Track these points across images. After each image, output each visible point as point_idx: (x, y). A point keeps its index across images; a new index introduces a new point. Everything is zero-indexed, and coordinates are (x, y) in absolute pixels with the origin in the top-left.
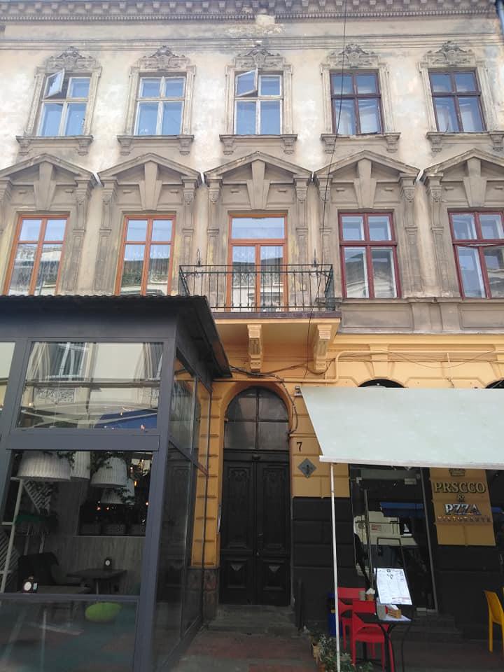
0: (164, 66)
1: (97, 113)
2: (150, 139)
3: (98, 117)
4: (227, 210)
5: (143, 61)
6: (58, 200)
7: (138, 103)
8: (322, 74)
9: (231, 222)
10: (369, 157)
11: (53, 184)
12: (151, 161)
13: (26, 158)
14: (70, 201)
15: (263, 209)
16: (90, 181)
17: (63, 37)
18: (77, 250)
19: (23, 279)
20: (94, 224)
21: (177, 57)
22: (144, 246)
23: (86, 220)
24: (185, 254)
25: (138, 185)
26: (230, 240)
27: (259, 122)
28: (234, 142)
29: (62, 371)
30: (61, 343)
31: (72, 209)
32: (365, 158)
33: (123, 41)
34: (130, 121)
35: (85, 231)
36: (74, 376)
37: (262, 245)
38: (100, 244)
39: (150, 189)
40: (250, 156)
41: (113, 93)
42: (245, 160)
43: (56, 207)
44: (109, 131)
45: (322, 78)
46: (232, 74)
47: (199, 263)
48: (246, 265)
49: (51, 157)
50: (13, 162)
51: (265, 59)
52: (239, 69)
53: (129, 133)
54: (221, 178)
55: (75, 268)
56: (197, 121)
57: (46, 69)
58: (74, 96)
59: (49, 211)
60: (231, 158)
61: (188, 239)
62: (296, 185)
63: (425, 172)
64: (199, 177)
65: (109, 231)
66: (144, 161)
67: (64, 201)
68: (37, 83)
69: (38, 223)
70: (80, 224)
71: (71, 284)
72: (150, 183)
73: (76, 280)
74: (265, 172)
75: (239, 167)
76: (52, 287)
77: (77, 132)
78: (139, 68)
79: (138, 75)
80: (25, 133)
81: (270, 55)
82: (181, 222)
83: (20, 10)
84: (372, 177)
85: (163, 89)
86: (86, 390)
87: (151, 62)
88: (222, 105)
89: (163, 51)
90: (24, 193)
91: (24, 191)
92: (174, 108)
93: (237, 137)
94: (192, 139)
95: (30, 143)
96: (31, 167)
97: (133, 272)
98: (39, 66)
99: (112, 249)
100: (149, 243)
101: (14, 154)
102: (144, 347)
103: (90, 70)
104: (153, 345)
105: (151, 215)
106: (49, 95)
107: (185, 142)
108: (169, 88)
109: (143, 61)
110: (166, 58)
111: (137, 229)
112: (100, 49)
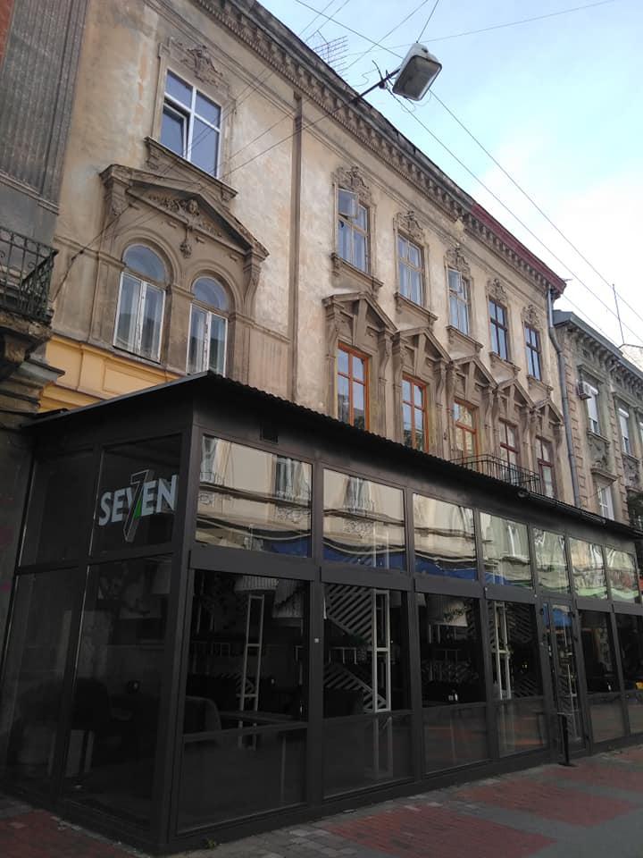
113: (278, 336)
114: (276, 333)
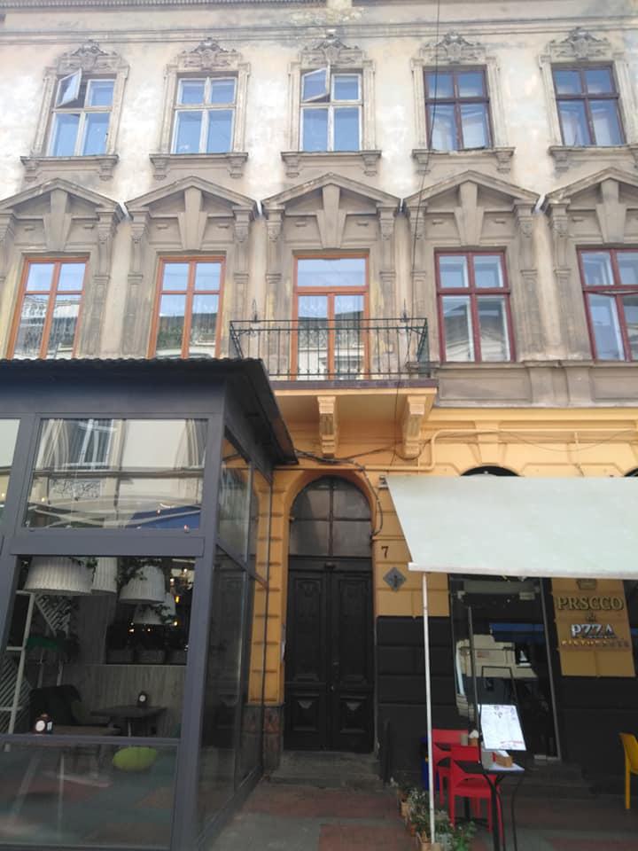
0: (210, 63)
2: (192, 159)
3: (125, 131)
5: (182, 57)
8: (413, 72)
11: (68, 218)
12: (193, 187)
13: (33, 185)
14: (91, 240)
15: (338, 247)
16: (115, 213)
17: (79, 28)
18: (100, 302)
20: (121, 267)
23: (111, 263)
26: (295, 288)
28: (299, 161)
29: (83, 457)
31: (93, 250)
34: (166, 135)
35: (109, 277)
36: (99, 464)
39: (192, 222)
40: (321, 179)
46: (296, 73)
50: (17, 190)
51: (340, 53)
52: (305, 66)
53: (165, 151)
55: (97, 325)
56: (254, 133)
59: (64, 253)
61: (241, 287)
64: (119, 208)
65: (245, 277)
66: (184, 187)
68: (46, 88)
69: (185, 268)
70: (103, 270)
72: (192, 217)
73: (99, 340)
78: (177, 67)
79: (175, 76)
80: (31, 152)
81: (103, 54)
84: (340, 207)
85: (208, 94)
87: (192, 60)
90: (31, 230)
92: (222, 118)
93: (304, 154)
95: (38, 165)
97: (171, 330)
98: (50, 66)
101: (18, 180)
102: (187, 425)
103: (114, 70)
104: (198, 423)
105: (194, 257)
106: (63, 102)
107: (237, 162)
108: (215, 92)
109: (182, 57)
110: (212, 54)
111: (176, 275)
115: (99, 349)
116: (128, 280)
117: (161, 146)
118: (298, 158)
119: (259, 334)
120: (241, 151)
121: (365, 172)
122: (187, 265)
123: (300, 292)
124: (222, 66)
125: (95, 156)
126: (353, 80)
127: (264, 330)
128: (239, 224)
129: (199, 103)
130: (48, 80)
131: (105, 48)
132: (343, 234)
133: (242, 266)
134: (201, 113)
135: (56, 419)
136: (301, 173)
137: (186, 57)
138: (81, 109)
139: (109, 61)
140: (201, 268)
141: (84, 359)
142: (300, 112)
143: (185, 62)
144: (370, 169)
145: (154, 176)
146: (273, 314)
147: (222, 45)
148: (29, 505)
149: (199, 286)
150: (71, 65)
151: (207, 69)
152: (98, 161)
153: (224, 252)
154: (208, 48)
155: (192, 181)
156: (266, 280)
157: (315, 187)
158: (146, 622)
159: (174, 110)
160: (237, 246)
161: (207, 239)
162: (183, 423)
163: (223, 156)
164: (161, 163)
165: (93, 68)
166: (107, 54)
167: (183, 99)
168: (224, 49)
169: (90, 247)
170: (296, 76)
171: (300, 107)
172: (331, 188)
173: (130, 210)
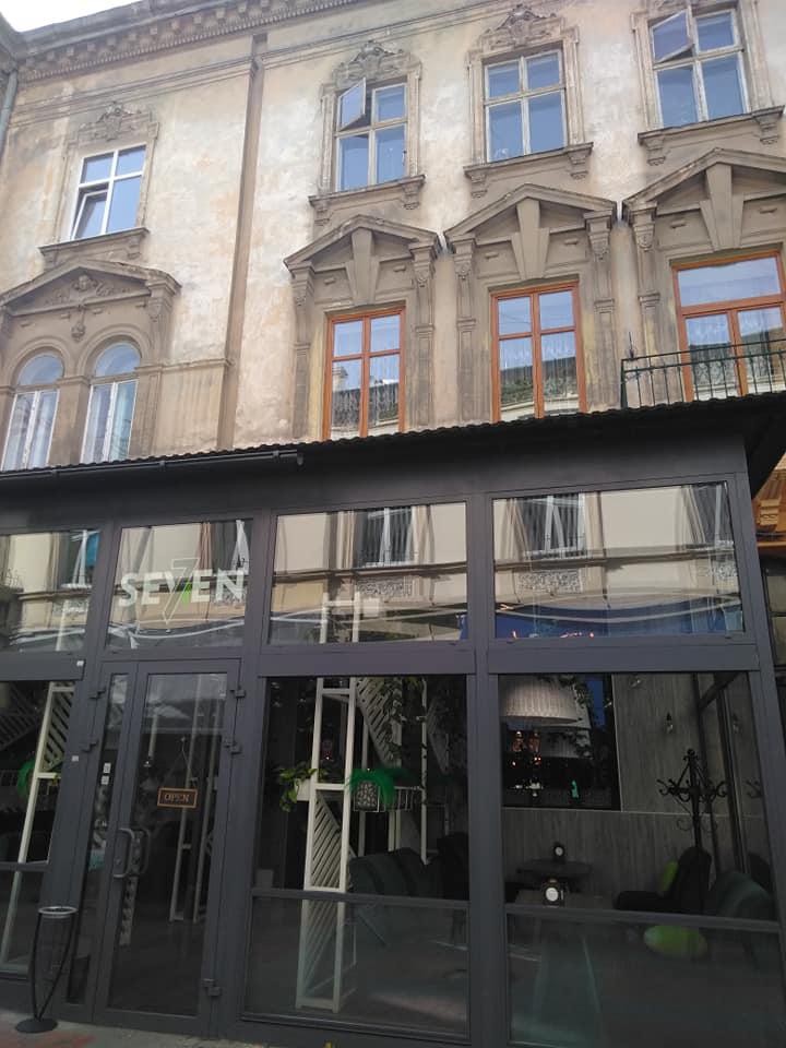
0: (523, 39)
1: (426, 137)
2: (518, 163)
3: (427, 144)
4: (486, 287)
5: (485, 38)
6: (556, 259)
7: (487, 108)
8: (634, 31)
9: (675, 278)
10: (366, 225)
11: (375, 262)
12: (528, 197)
13: (326, 230)
14: (403, 285)
15: (736, 246)
16: (433, 247)
17: (355, 28)
18: (426, 359)
19: (341, 418)
20: (445, 315)
21: (544, 18)
22: (397, 356)
23: (433, 309)
24: (604, 341)
25: (510, 242)
26: (679, 309)
27: (704, 98)
28: (664, 140)
29: (548, 543)
30: (537, 497)
31: (409, 298)
32: (718, 163)
33: (448, 13)
34: (479, 140)
35: (433, 326)
36: (568, 549)
37: (740, 309)
38: (460, 345)
39: (531, 243)
40: (703, 159)
41: (447, 100)
42: (695, 166)
43: (383, 296)
44: (449, 161)
45: (635, 37)
46: (643, 26)
47: (632, 355)
48: (716, 347)
49: (369, 218)
50: (308, 237)
51: (380, 62)
52: (654, 14)
53: (481, 160)
54: (655, 205)
55: (426, 387)
56: (594, 117)
57: (335, 84)
58: (380, 119)
59: (373, 306)
60: (665, 170)
61: (606, 317)
62: (589, 230)
63: (624, 206)
64: (437, 239)
65: (472, 323)
66: (516, 200)
67: (394, 285)
68: (326, 109)
69: (357, 327)
70: (425, 319)
71: (424, 414)
72: (531, 236)
73: (431, 406)
74: (733, 181)
75: (685, 181)
76: (393, 424)
77: (392, 176)
78: (482, 51)
79: (480, 63)
80: (319, 190)
81: (387, 54)
82: (588, 291)
83: (70, 58)
84: (734, 193)
85: (524, 77)
86: (598, 569)
87: (499, 38)
88: (633, 84)
89: (519, 14)
90: (333, 282)
91: (332, 279)
92: (550, 106)
93: (671, 131)
94: (588, 150)
95: (329, 204)
96: (339, 240)
97: (518, 383)
98: (323, 82)
99: (480, 348)
100: (536, 334)
101: (309, 226)
102: (508, 506)
103: (403, 71)
104: (522, 501)
105: (534, 288)
106: (343, 127)
107: (578, 156)
108: (531, 73)
109: (485, 38)
110: (526, 25)
111: (515, 312)
112: (414, 33)
113: (205, 364)
114: (207, 361)
115: (433, 417)
116: (294, 351)
117: (474, 155)
118: (661, 138)
119: (752, 362)
120: (581, 142)
121: (405, 206)
122: (527, 299)
123: (686, 314)
124: (540, 38)
125: (396, 181)
126: (721, 20)
127: (744, 357)
128: (595, 237)
129: (512, 91)
130: (326, 99)
131: (389, 47)
132: (742, 227)
133: (603, 292)
134: (519, 104)
135: (346, 511)
136: (669, 156)
137: (491, 36)
138: (368, 127)
139: (396, 61)
140: (545, 300)
141: (382, 436)
142: (484, 113)
143: (491, 42)
144: (768, 134)
145: (472, 194)
146: (657, 347)
147: (536, 12)
148: (498, 606)
149: (376, 347)
150: (351, 75)
151: (520, 46)
152: (401, 186)
153: (577, 276)
154: (520, 18)
155: (527, 190)
156: (458, 328)
157: (696, 171)
158: (563, 755)
159: (484, 107)
160: (596, 265)
161: (550, 264)
162: (676, 490)
163: (560, 152)
164: (479, 176)
165: (377, 73)
166: (392, 54)
167: (380, 115)
168: (541, 16)
169: (578, 267)
170: (642, 31)
171: (484, 107)
172: (717, 168)
173: (451, 240)
